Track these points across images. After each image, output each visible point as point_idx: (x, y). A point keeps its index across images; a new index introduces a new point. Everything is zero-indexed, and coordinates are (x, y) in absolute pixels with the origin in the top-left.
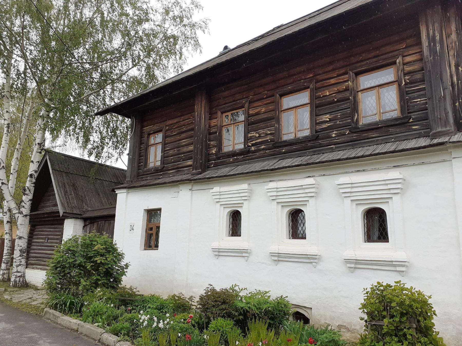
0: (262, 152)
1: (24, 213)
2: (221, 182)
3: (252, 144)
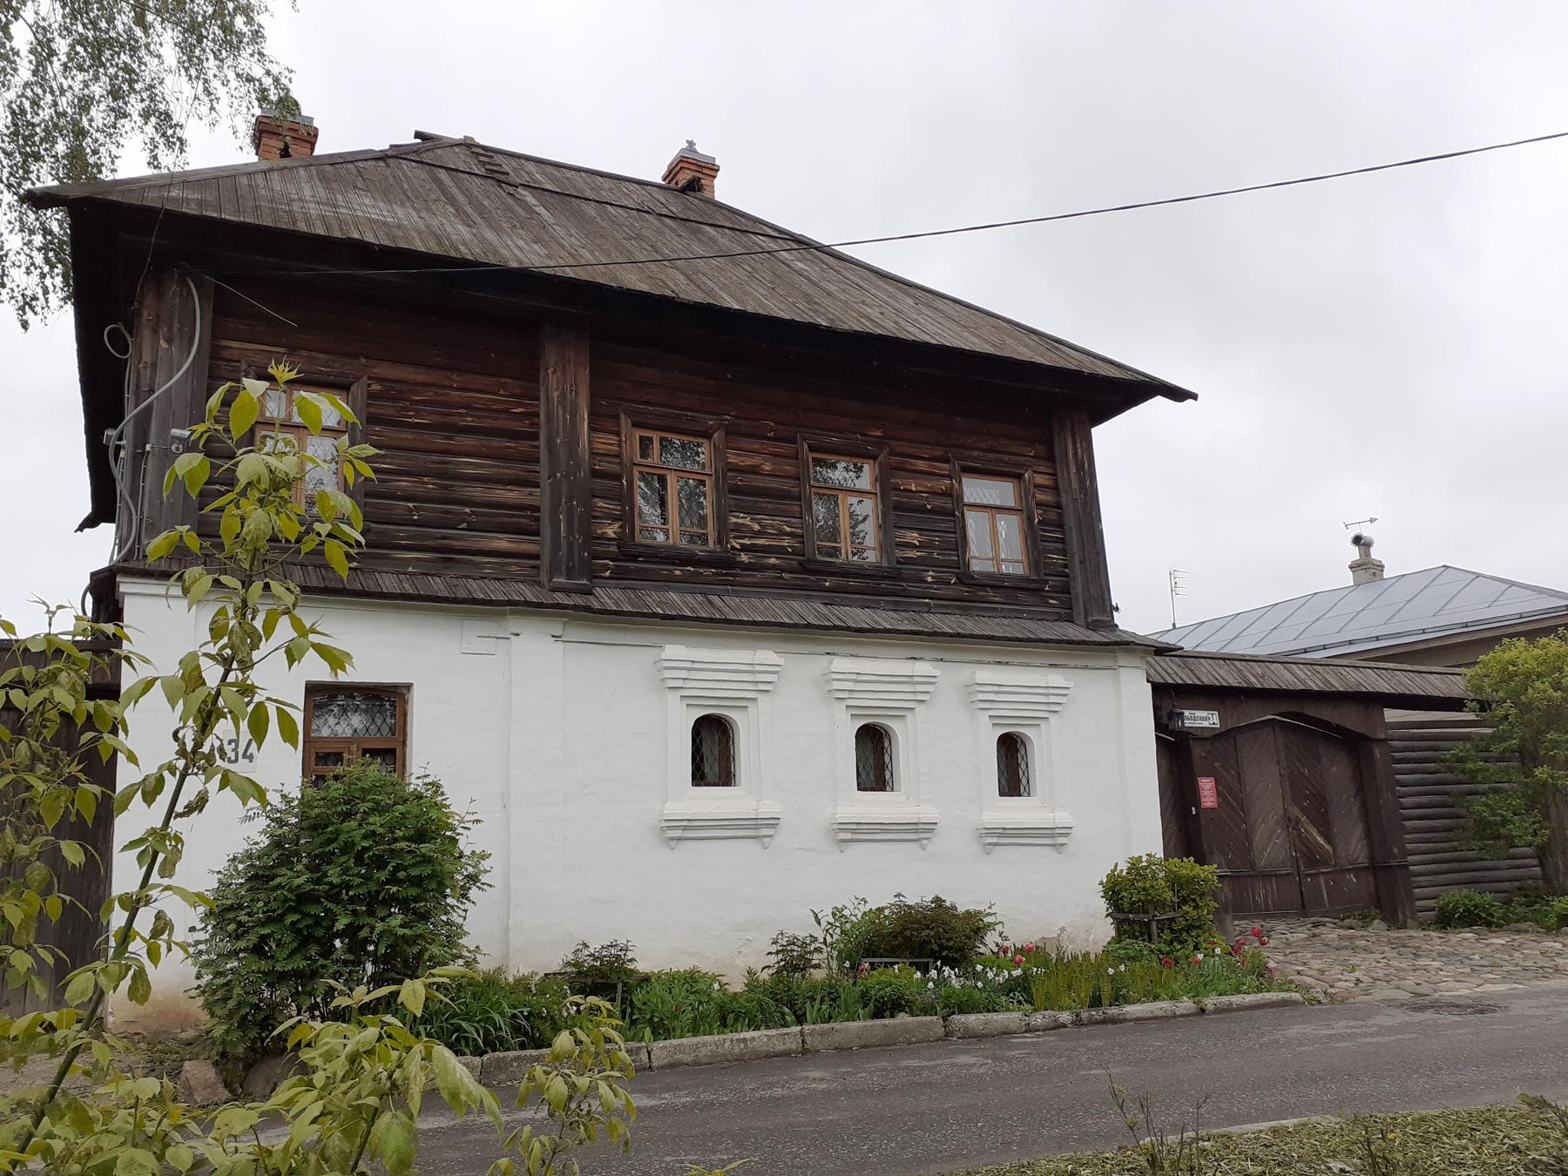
2: (786, 640)
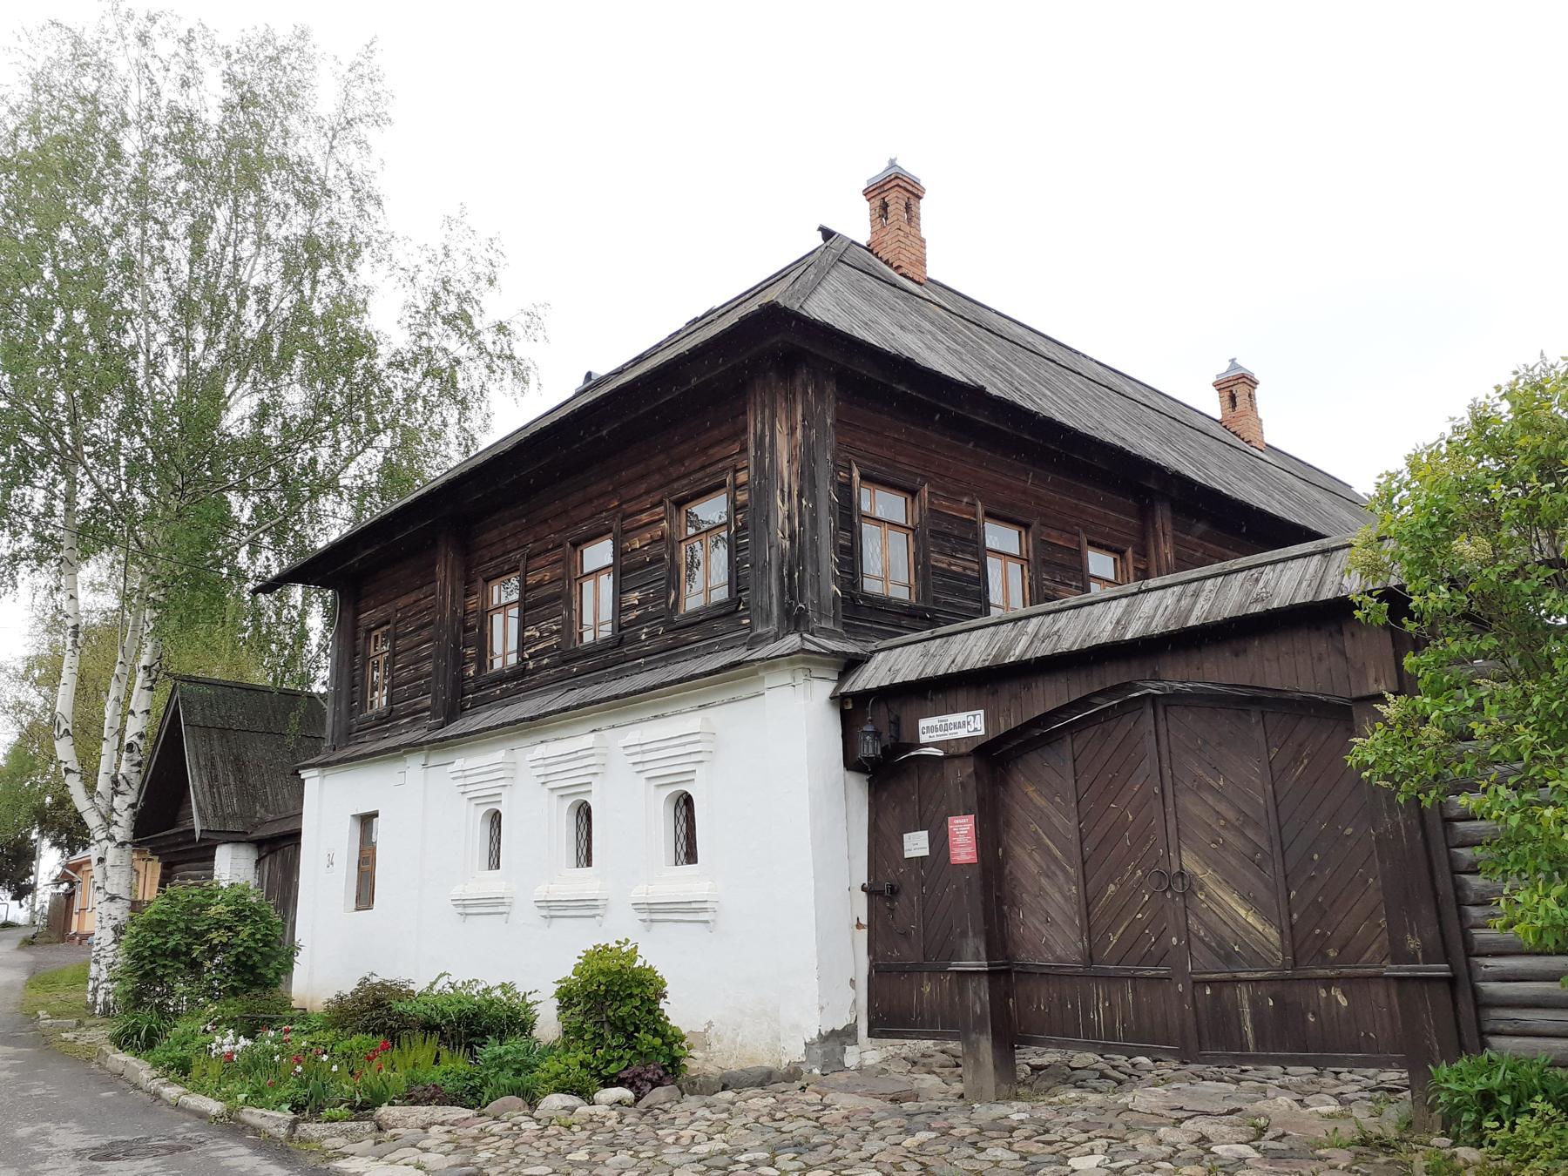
0: (544, 673)
1: (119, 839)
3: (530, 654)
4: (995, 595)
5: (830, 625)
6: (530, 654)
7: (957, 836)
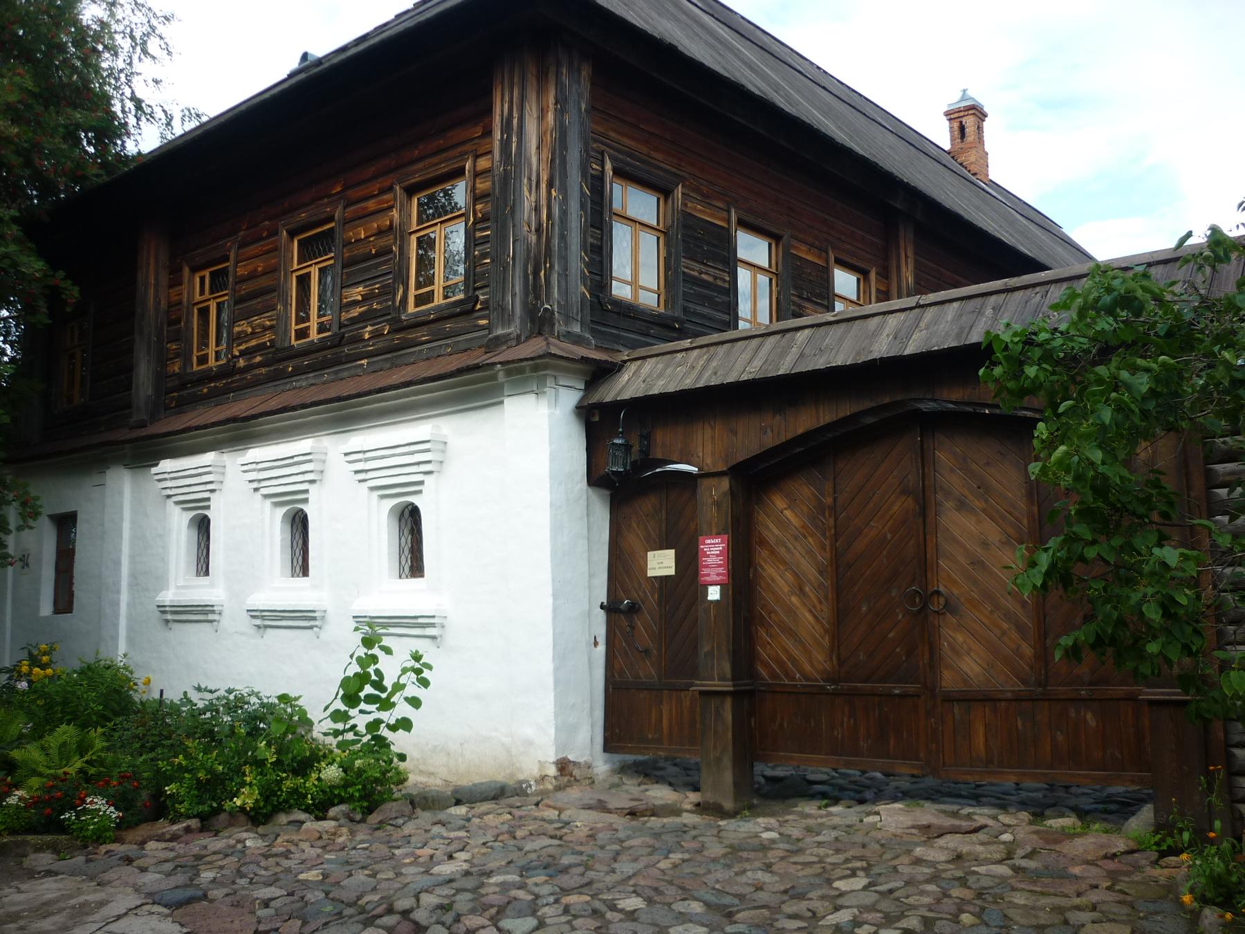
0: (257, 372)
3: (240, 351)
4: (744, 308)
5: (576, 328)
6: (240, 351)
7: (708, 556)
